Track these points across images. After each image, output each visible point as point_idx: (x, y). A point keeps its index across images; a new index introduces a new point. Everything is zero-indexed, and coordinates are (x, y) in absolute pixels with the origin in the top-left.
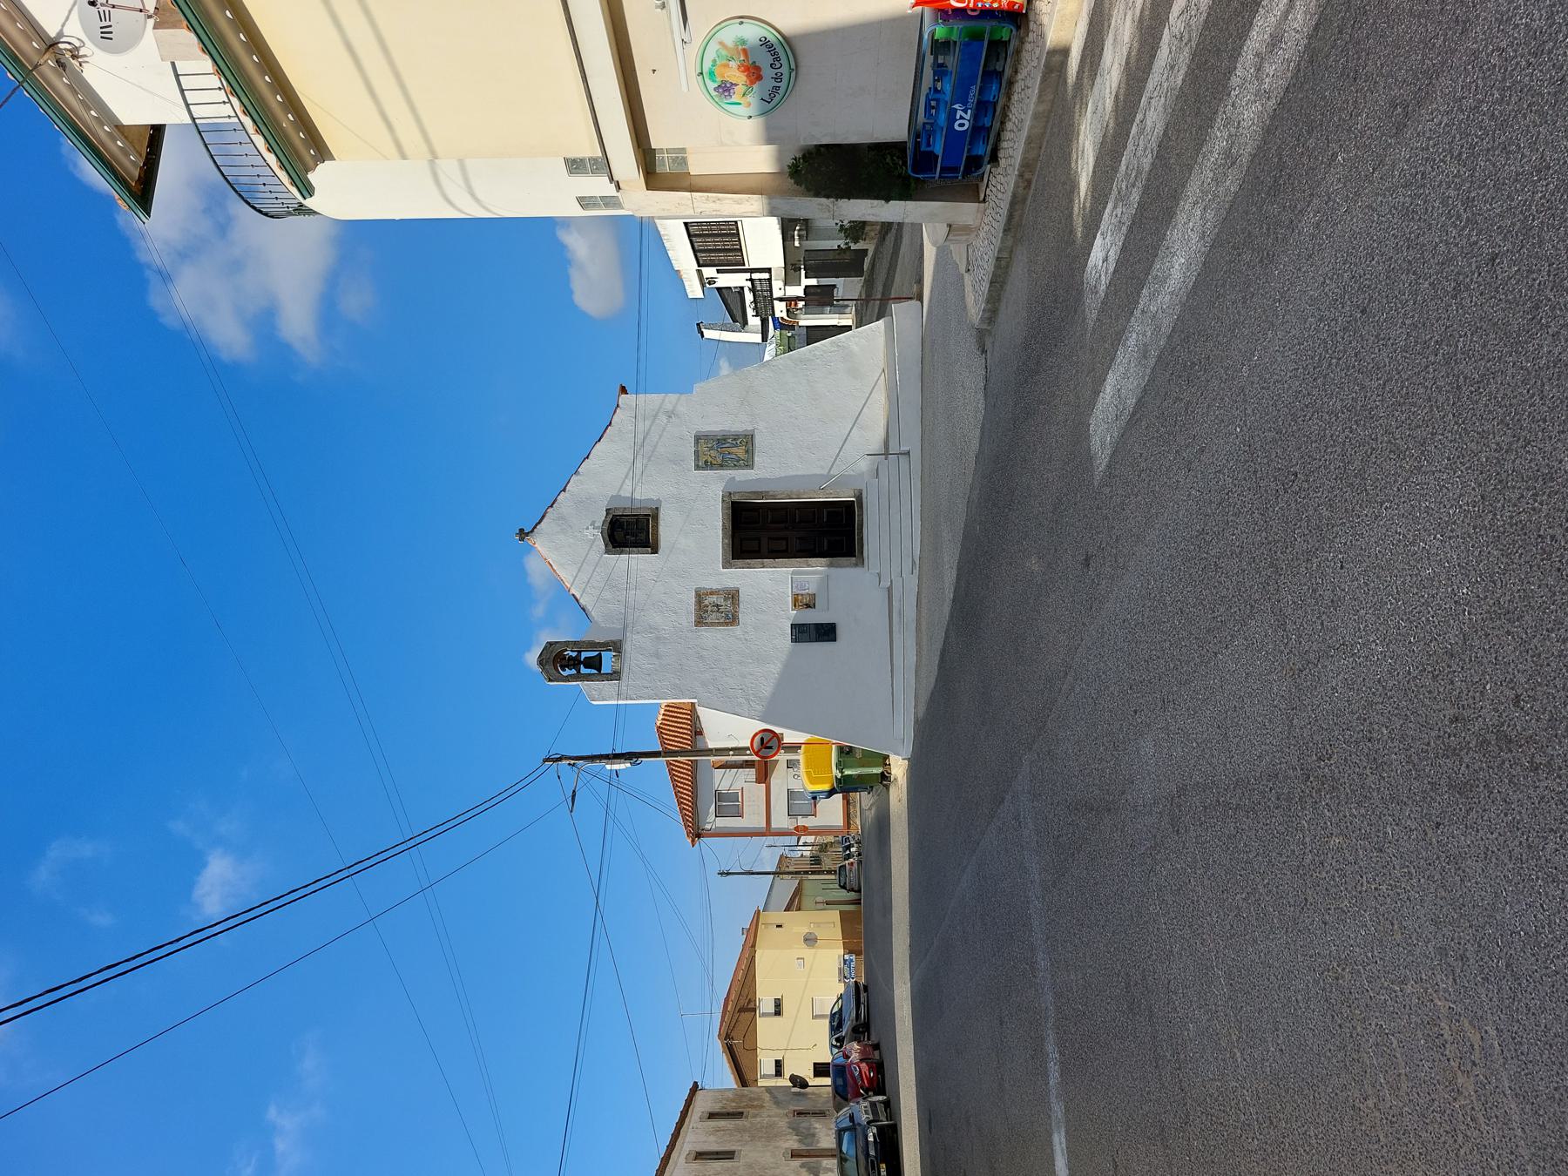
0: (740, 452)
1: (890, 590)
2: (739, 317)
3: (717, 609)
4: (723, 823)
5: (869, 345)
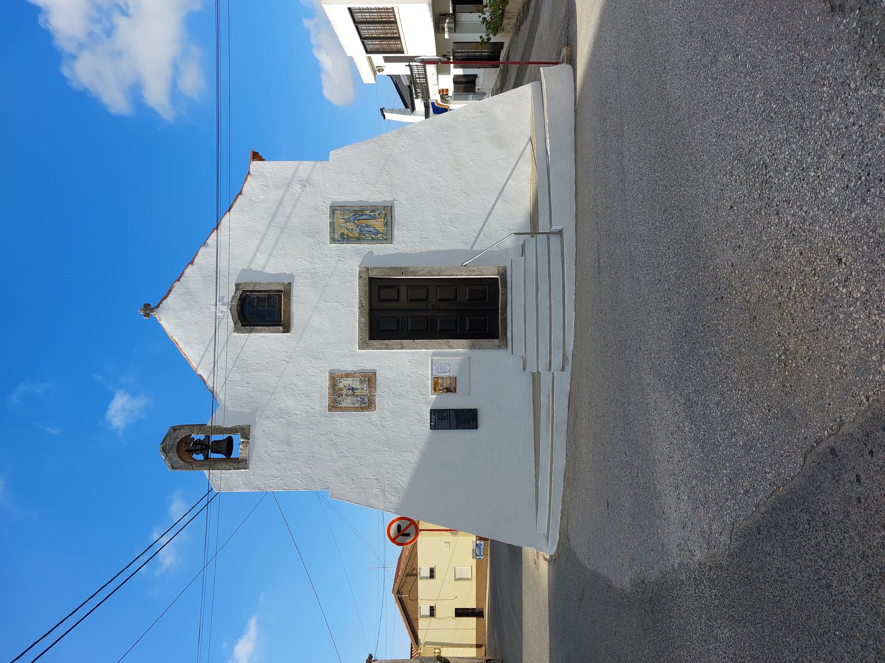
0: (378, 225)
1: (536, 378)
2: (409, 105)
3: (352, 394)
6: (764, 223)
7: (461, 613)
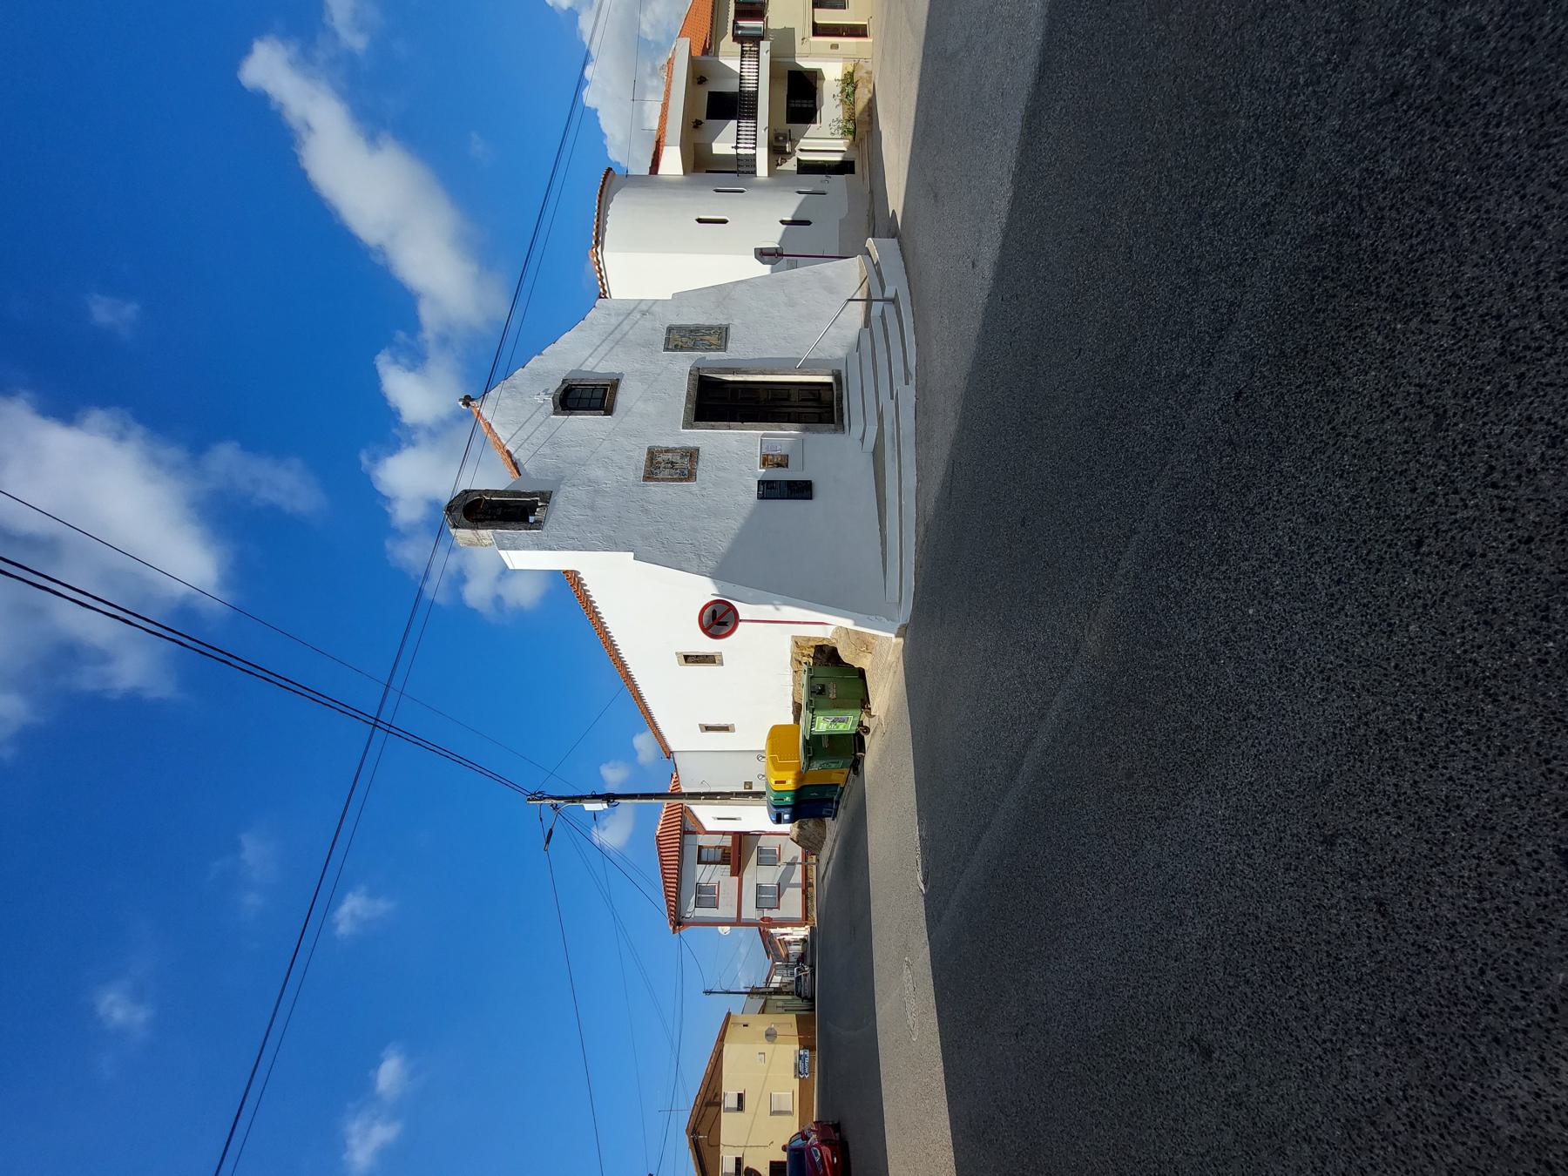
0: (714, 339)
4: (702, 913)
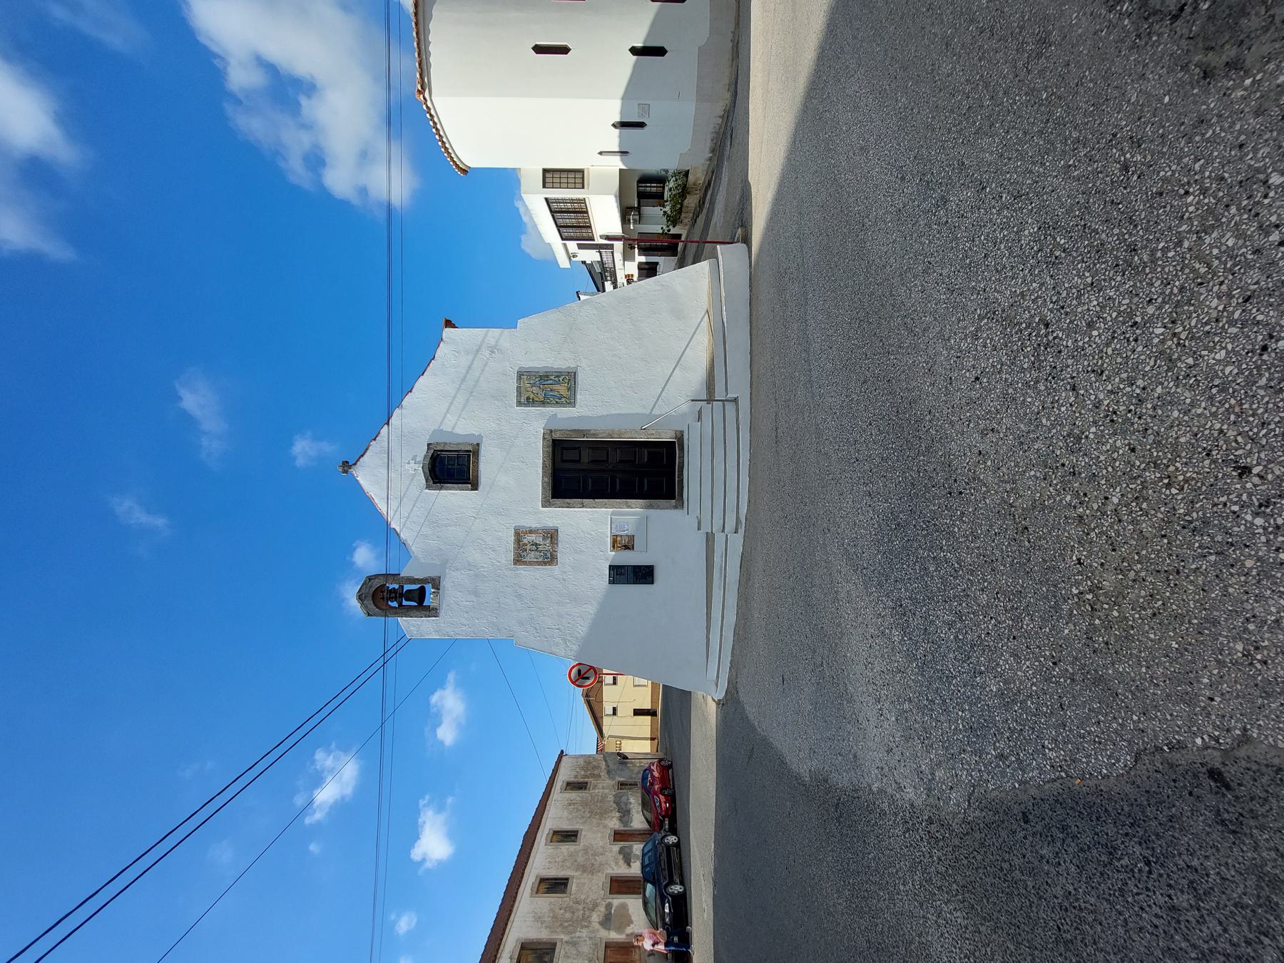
0: (562, 389)
1: (710, 538)
3: (536, 549)
5: (690, 283)
6: (1044, 402)
7: (637, 712)
